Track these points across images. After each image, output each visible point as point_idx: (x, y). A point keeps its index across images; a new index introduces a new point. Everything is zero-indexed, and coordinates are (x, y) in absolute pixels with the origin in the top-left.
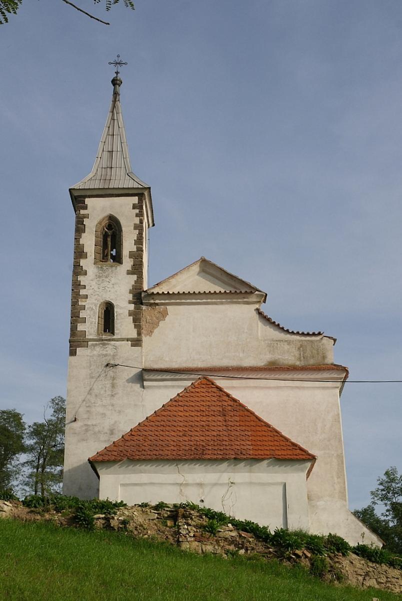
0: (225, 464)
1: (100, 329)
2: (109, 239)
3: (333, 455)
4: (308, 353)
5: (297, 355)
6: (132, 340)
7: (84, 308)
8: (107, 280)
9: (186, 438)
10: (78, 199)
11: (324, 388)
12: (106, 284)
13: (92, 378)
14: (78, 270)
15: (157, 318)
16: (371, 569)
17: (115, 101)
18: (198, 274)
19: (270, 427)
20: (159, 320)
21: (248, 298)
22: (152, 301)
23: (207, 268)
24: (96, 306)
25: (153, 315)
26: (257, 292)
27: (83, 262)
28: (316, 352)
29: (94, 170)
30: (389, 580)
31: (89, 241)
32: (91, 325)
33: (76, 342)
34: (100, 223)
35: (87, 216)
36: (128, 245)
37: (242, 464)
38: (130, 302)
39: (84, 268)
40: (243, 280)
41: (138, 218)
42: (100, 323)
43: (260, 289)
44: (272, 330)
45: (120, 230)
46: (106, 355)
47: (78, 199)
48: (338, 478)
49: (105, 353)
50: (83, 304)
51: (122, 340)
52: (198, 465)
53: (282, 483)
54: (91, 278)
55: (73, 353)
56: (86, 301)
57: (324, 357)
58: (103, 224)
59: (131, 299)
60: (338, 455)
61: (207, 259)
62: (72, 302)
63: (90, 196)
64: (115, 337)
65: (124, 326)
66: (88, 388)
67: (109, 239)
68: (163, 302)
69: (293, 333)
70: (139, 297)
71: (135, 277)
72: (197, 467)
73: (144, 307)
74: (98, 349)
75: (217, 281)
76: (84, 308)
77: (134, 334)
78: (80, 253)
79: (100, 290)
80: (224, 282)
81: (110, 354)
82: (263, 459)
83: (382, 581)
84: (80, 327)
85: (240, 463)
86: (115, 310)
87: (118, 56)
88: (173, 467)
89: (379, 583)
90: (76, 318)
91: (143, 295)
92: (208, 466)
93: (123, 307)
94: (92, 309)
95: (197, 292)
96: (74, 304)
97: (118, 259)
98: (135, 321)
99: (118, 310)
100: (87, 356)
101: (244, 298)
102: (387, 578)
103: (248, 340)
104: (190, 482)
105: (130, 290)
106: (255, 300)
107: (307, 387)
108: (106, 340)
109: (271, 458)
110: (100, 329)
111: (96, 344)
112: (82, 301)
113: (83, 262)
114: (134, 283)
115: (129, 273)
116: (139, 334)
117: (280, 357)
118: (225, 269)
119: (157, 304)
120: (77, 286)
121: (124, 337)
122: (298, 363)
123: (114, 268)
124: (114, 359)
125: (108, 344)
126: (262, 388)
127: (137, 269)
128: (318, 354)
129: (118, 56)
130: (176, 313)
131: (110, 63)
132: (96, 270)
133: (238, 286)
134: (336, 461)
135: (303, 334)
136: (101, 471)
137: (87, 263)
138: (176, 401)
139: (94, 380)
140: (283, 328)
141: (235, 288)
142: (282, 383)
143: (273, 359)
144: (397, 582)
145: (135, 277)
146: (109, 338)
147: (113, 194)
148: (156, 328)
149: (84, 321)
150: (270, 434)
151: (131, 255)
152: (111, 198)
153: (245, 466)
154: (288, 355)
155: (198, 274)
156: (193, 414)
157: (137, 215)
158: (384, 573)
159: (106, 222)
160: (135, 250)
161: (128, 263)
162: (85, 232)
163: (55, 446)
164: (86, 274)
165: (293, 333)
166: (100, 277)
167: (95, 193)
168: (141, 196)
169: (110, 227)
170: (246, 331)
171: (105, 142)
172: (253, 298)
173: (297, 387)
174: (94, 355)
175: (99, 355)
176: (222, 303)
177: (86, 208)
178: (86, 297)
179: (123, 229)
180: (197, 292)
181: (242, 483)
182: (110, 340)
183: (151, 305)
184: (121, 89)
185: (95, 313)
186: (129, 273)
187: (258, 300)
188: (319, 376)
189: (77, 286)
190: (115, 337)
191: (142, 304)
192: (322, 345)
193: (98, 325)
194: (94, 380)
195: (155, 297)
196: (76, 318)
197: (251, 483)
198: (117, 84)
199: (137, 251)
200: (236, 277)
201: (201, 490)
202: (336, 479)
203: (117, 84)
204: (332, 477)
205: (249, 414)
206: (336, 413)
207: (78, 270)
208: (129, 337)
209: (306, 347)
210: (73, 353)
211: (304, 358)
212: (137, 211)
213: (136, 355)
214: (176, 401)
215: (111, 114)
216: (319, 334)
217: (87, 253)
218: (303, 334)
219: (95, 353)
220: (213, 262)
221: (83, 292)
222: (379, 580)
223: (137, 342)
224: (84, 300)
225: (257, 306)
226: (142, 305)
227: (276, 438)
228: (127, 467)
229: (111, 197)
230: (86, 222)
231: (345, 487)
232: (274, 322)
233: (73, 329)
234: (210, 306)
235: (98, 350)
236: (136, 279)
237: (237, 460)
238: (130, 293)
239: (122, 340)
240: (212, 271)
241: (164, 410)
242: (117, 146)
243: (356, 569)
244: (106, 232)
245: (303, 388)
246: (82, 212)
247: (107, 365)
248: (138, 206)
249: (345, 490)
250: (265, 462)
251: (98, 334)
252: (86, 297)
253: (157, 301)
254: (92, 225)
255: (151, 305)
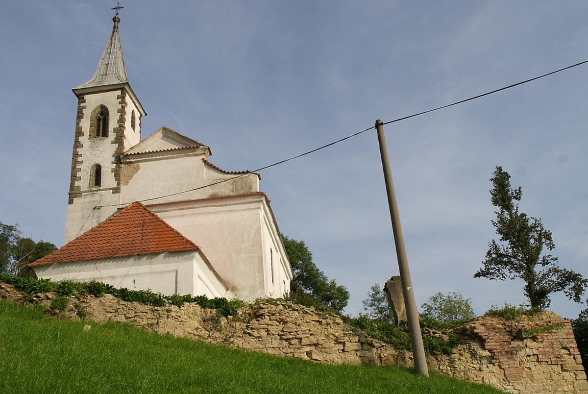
0: (132, 260)
1: (91, 183)
2: (101, 122)
3: (255, 256)
4: (239, 186)
5: (231, 188)
6: (113, 189)
7: (80, 170)
8: (97, 149)
9: (108, 245)
10: (80, 95)
11: (249, 209)
12: (96, 152)
13: (84, 218)
14: (77, 144)
15: (132, 172)
16: (122, 306)
17: (114, 32)
18: (162, 139)
19: (173, 231)
20: (133, 173)
21: (195, 151)
22: (128, 161)
23: (168, 133)
24: (88, 168)
25: (129, 170)
26: (201, 147)
27: (81, 139)
28: (245, 185)
29: (94, 77)
30: (137, 314)
31: (86, 125)
32: (84, 180)
33: (74, 193)
34: (94, 111)
35: (85, 107)
36: (113, 124)
37: (145, 258)
38: (113, 163)
39: (81, 143)
40: (192, 139)
41: (121, 105)
42: (91, 179)
43: (204, 144)
44: (214, 172)
45: (108, 114)
46: (94, 201)
47: (80, 95)
48: (258, 273)
49: (93, 200)
50: (80, 167)
51: (106, 189)
52: (111, 262)
53: (175, 270)
54: (85, 149)
55: (71, 202)
56: (81, 165)
57: (250, 188)
58: (97, 112)
59: (114, 161)
60: (259, 257)
61: (166, 127)
62: (72, 167)
63: (88, 94)
64: (101, 188)
65: (108, 179)
66: (80, 226)
67: (101, 122)
68: (136, 160)
69: (228, 173)
70: (120, 158)
71: (117, 145)
72: (110, 264)
73: (123, 166)
74: (88, 197)
75: (175, 142)
76: (80, 170)
77: (115, 185)
78: (79, 133)
79: (92, 157)
80: (180, 143)
81: (97, 201)
82: (159, 254)
83: (130, 316)
84: (77, 184)
85: (142, 258)
86: (102, 169)
87: (118, 3)
88: (92, 265)
89: (127, 318)
90: (74, 177)
91: (121, 157)
92: (119, 262)
93: (108, 167)
94: (86, 170)
95: (159, 151)
96: (74, 168)
97: (105, 134)
98: (115, 176)
99: (104, 169)
100: (81, 203)
101: (193, 152)
102: (136, 313)
103: (196, 181)
104: (105, 276)
105: (113, 154)
106: (201, 152)
107: (237, 210)
108: (95, 191)
109: (165, 252)
110: (91, 183)
111: (88, 194)
112: (78, 166)
113: (81, 139)
114: (116, 150)
115: (113, 143)
116: (118, 184)
117: (218, 191)
118: (179, 133)
119: (131, 162)
120: (76, 155)
121: (107, 188)
122: (232, 194)
123: (102, 140)
124: (99, 203)
125: (95, 193)
126: (204, 214)
127: (120, 139)
128: (246, 186)
129: (118, 3)
130: (146, 168)
131: (520, 188)
132: (89, 143)
133: (189, 144)
134: (257, 261)
135: (236, 173)
136: (39, 273)
137: (84, 140)
138: (110, 220)
139: (85, 220)
140: (221, 170)
141: (188, 146)
142: (219, 209)
143: (214, 193)
144: (145, 316)
145: (117, 145)
146: (97, 189)
147: (103, 91)
148: (130, 179)
149: (80, 179)
150: (173, 236)
151: (115, 130)
152: (101, 94)
153: (147, 260)
154: (225, 189)
155: (162, 139)
156: (119, 227)
157: (120, 103)
158: (134, 309)
159: (99, 110)
160: (118, 127)
161: (112, 136)
162: (83, 118)
163: (460, 350)
164: (83, 147)
165: (228, 173)
166: (92, 147)
167: (91, 91)
168: (123, 89)
169: (102, 113)
170: (194, 175)
171: (104, 59)
172: (199, 151)
173: (230, 211)
174: (86, 202)
175: (89, 202)
176: (178, 157)
177: (84, 102)
178: (82, 162)
179: (110, 113)
180: (159, 151)
181: (144, 274)
182: (97, 191)
183: (128, 163)
184: (120, 25)
185: (87, 173)
186: (113, 143)
187: (203, 152)
188: (242, 201)
189: (76, 155)
190: (101, 188)
191: (121, 163)
192: (249, 179)
193: (90, 182)
194: (85, 220)
195: (129, 157)
196: (74, 177)
197: (151, 273)
198: (116, 21)
199: (119, 127)
200: (186, 138)
201: (113, 281)
202: (257, 273)
203: (116, 21)
204: (254, 273)
205: (164, 226)
206: (258, 227)
207: (77, 144)
208: (111, 187)
209: (238, 182)
210: (71, 202)
211: (236, 189)
212: (120, 100)
213: (115, 199)
214: (110, 220)
215: (110, 40)
216: (248, 172)
217: (84, 132)
218: (236, 173)
219: (87, 200)
220: (171, 129)
221: (79, 159)
222: (127, 315)
223: (116, 190)
224: (80, 164)
225: (204, 157)
226: (122, 164)
227: (176, 238)
228: (58, 268)
229: (102, 92)
230: (84, 111)
231: (263, 279)
232: (218, 168)
233: (72, 185)
234: (170, 160)
235: (89, 199)
236: (117, 147)
237: (140, 255)
238: (113, 156)
239: (106, 189)
240: (171, 135)
241: (99, 227)
242: (112, 60)
243: (105, 308)
244: (99, 117)
245: (234, 211)
246: (82, 105)
247: (94, 208)
248: (122, 97)
249: (263, 281)
250: (162, 255)
251: (90, 187)
252: (82, 162)
253: (132, 160)
254: (88, 113)
255: (128, 163)
